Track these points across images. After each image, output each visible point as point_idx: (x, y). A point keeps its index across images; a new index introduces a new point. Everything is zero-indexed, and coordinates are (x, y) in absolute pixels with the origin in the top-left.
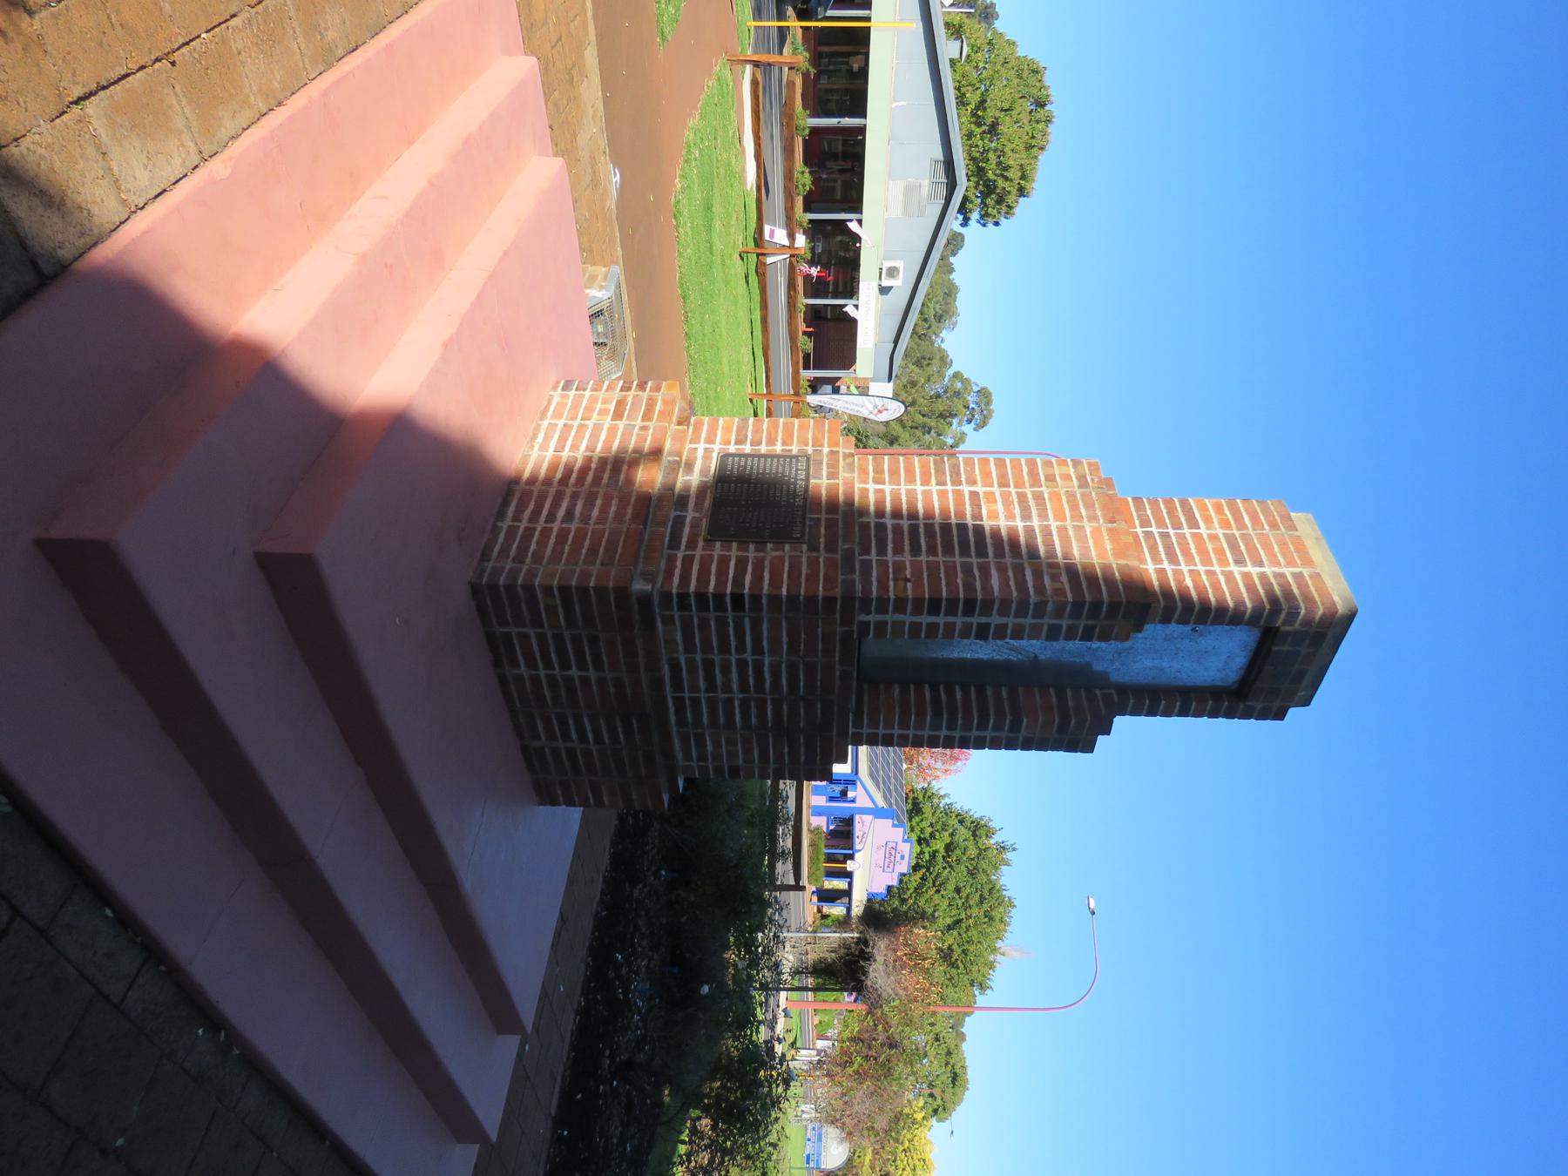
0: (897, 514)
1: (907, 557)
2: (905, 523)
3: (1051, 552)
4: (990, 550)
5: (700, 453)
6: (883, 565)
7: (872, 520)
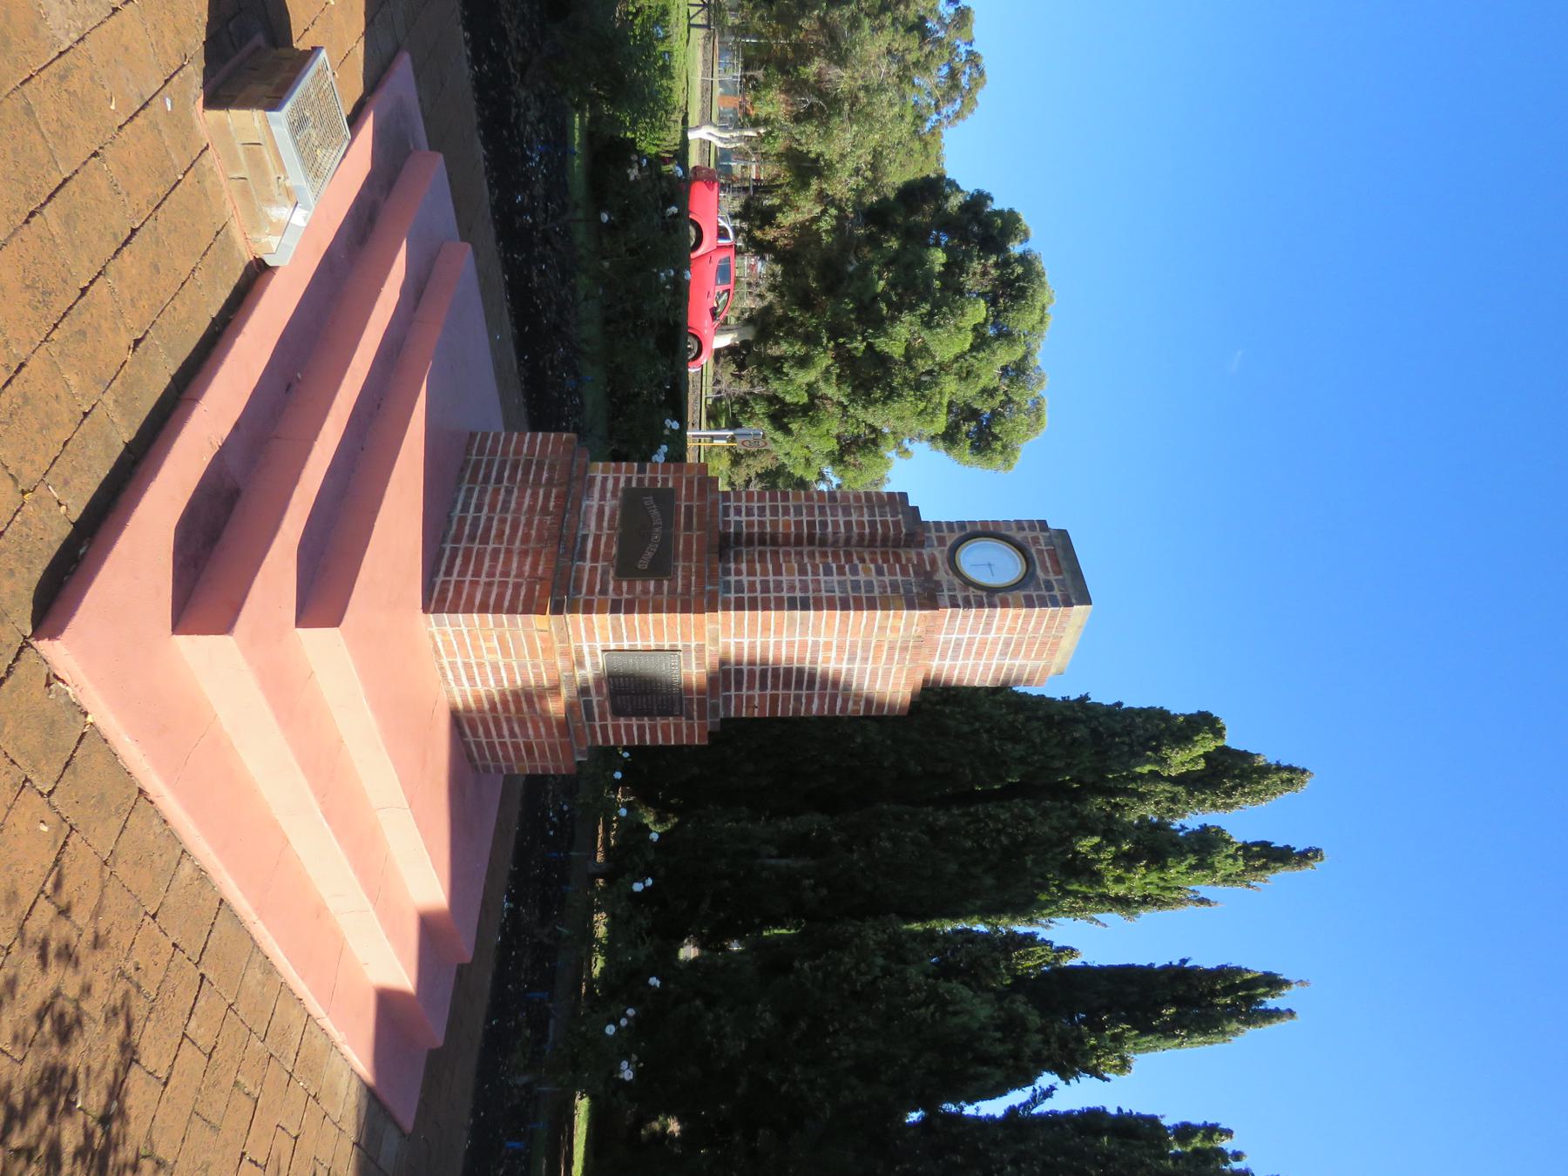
0: (752, 663)
1: (757, 692)
2: (758, 669)
3: (860, 686)
4: (817, 686)
5: (586, 651)
6: (739, 698)
7: (733, 668)
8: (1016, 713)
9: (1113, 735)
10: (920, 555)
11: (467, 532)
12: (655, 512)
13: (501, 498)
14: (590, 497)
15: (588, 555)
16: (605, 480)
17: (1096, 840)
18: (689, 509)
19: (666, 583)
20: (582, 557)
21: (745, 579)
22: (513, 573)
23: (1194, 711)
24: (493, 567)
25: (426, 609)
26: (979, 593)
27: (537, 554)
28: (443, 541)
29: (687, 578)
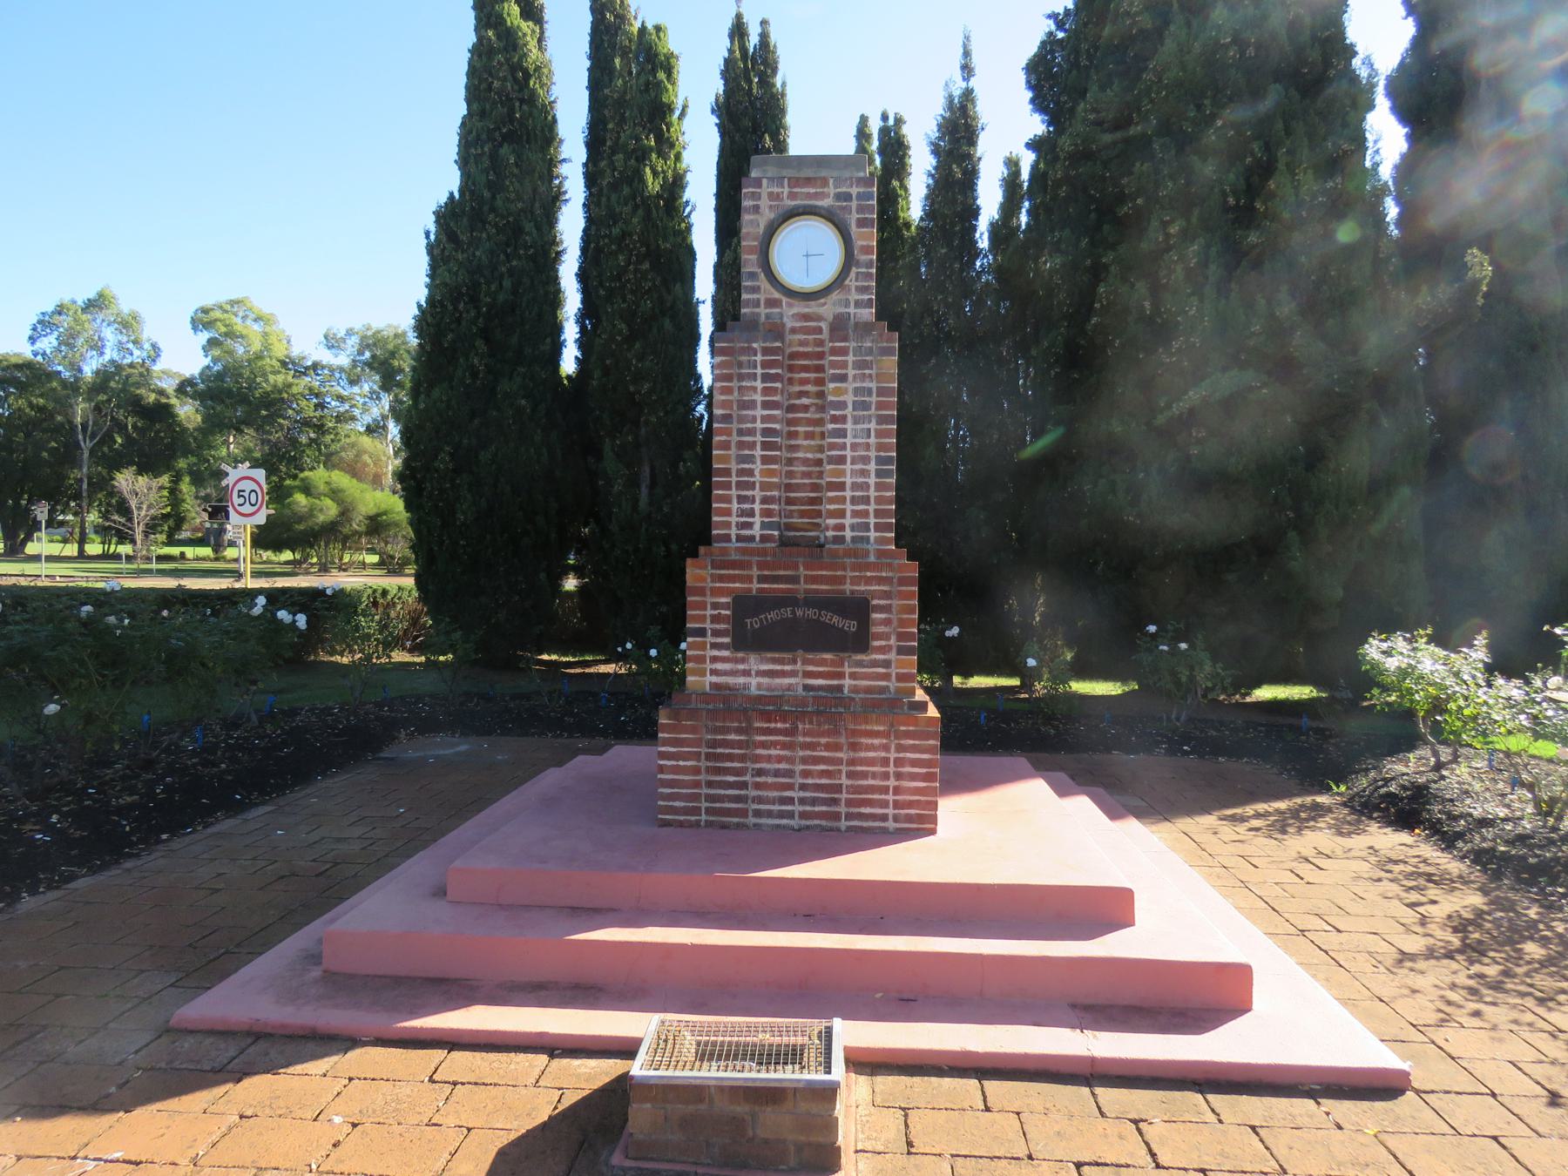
8: (484, 222)
9: (512, 119)
10: (794, 331)
11: (824, 808)
12: (772, 616)
13: (770, 780)
14: (746, 687)
15: (835, 682)
16: (714, 672)
17: (648, 170)
18: (762, 579)
19: (875, 602)
20: (840, 688)
21: (848, 521)
22: (883, 754)
23: (472, 14)
24: (874, 776)
25: (933, 832)
26: (852, 275)
27: (854, 733)
28: (838, 830)
29: (869, 581)
